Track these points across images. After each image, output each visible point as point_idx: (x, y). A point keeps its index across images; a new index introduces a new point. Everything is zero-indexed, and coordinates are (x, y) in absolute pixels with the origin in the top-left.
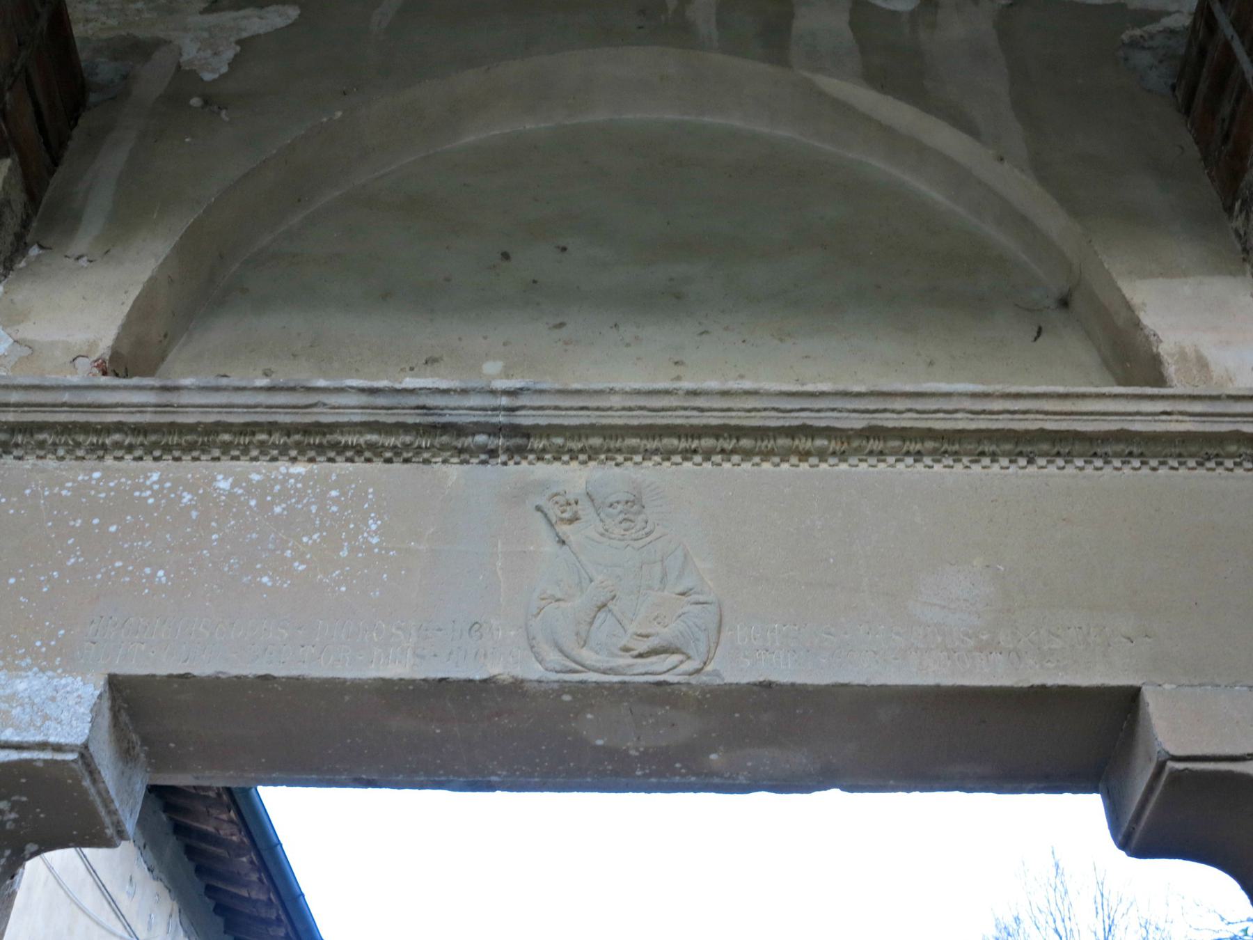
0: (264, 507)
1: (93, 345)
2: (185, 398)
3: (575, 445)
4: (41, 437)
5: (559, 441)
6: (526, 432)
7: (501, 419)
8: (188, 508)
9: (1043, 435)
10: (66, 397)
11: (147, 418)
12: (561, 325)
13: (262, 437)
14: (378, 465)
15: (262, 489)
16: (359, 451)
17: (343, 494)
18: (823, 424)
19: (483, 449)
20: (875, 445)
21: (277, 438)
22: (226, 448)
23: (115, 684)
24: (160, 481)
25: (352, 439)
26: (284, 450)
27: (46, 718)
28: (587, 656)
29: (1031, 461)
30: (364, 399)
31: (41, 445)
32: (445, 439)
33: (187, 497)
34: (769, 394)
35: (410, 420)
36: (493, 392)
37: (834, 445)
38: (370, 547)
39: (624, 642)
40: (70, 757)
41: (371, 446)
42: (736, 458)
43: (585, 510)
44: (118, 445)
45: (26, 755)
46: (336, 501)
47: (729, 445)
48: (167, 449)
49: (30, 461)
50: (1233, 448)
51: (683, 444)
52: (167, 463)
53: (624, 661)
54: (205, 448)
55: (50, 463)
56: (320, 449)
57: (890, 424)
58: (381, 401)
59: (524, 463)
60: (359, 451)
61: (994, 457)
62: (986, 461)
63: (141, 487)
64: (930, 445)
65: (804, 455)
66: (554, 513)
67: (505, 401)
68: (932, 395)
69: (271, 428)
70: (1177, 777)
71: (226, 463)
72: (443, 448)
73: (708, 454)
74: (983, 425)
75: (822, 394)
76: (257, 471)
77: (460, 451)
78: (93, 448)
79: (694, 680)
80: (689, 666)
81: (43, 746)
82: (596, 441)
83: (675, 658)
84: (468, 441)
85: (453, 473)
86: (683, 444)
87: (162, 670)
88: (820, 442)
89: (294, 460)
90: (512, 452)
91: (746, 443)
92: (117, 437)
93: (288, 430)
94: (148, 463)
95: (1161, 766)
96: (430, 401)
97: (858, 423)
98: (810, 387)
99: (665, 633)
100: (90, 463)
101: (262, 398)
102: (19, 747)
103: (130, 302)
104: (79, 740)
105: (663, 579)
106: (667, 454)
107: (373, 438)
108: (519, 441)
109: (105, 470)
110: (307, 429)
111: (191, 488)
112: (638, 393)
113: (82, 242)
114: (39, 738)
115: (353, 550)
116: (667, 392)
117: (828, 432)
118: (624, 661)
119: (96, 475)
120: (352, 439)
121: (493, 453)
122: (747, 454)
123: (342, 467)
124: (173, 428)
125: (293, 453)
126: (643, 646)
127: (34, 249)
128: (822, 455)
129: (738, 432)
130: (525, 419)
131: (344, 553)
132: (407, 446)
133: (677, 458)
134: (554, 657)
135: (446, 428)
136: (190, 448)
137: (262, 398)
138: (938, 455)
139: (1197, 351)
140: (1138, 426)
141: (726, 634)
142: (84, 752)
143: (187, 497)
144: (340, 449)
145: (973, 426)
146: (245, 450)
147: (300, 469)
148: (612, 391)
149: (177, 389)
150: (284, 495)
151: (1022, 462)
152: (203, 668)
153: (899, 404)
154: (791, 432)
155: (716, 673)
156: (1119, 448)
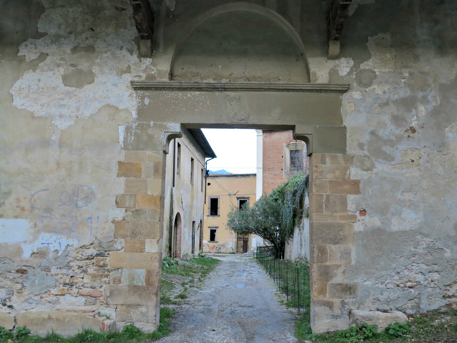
0: (195, 99)
1: (167, 70)
2: (183, 84)
3: (232, 90)
4: (165, 89)
5: (230, 89)
6: (226, 88)
7: (223, 87)
8: (185, 99)
9: (291, 89)
10: (168, 84)
11: (178, 87)
12: (229, 58)
13: (193, 89)
14: (208, 92)
15: (193, 96)
16: (205, 90)
17: (204, 97)
18: (263, 88)
19: (221, 90)
20: (270, 90)
21: (195, 89)
22: (189, 90)
23: (181, 124)
24: (181, 95)
25: (205, 89)
26: (196, 90)
27: (175, 129)
28: (234, 121)
29: (289, 92)
30: (206, 84)
31: (165, 90)
32: (216, 89)
33: (185, 97)
34: (256, 84)
35: (212, 87)
36: (222, 83)
37: (264, 90)
38: (208, 105)
39: (238, 119)
40: (178, 133)
41: (207, 90)
42: (252, 91)
43: (233, 99)
44: (175, 90)
45: (174, 133)
46: (203, 98)
47: (251, 90)
48: (181, 90)
49: (164, 91)
50: (315, 91)
51: (246, 90)
52: (181, 92)
53: (238, 121)
54: (186, 90)
55: (167, 92)
56: (200, 90)
57: (271, 88)
58: (208, 84)
59: (226, 92)
60: (205, 90)
61: (284, 91)
62: (283, 92)
63: (179, 96)
64: (276, 90)
65: (260, 91)
66: (230, 100)
67: (223, 84)
68: (277, 84)
69: (194, 88)
70: (297, 136)
71: (189, 92)
72: (216, 90)
73: (249, 91)
74: (283, 88)
75: (263, 84)
76: (193, 93)
77: (218, 91)
78: (172, 90)
79: (246, 124)
80: (245, 122)
81: (175, 132)
82: (235, 89)
83: (244, 121)
84: (219, 89)
85: (217, 93)
86: (246, 90)
87: (187, 123)
88: (263, 90)
89: (197, 92)
90: (224, 91)
91: (253, 90)
92: (175, 89)
93: (196, 88)
94: (179, 92)
95: (296, 135)
96: (214, 85)
97: (267, 87)
98: (261, 83)
99: (243, 118)
100: (172, 92)
101: (193, 84)
102: (173, 132)
103: (170, 62)
104: (179, 132)
105: (243, 111)
106: (244, 91)
107: (207, 89)
108: (225, 89)
109: (174, 93)
110: (199, 88)
111: (185, 96)
112: (240, 83)
113: (161, 49)
114: (175, 131)
115: (206, 105)
116: (244, 83)
117: (264, 89)
118: (238, 121)
119: (173, 94)
120: (205, 89)
121: (222, 91)
122: (253, 91)
123: (203, 92)
124: (182, 88)
125: (197, 91)
126: (240, 120)
127: (238, 206)
128: (263, 91)
129: (252, 89)
130: (226, 87)
131: (205, 106)
132: (211, 90)
133: (245, 91)
134: (230, 121)
135: (216, 88)
136: (184, 90)
137: (193, 84)
138: (277, 91)
139: (315, 72)
140: (303, 88)
141: (250, 117)
142: (180, 133)
143: (185, 97)
144: (203, 90)
145: (282, 88)
146: (191, 90)
147: (198, 93)
148: (237, 83)
149: (182, 83)
150: (197, 97)
151: (288, 92)
152: (191, 122)
153: (273, 85)
154: (259, 89)
155: (248, 123)
156: (300, 90)
